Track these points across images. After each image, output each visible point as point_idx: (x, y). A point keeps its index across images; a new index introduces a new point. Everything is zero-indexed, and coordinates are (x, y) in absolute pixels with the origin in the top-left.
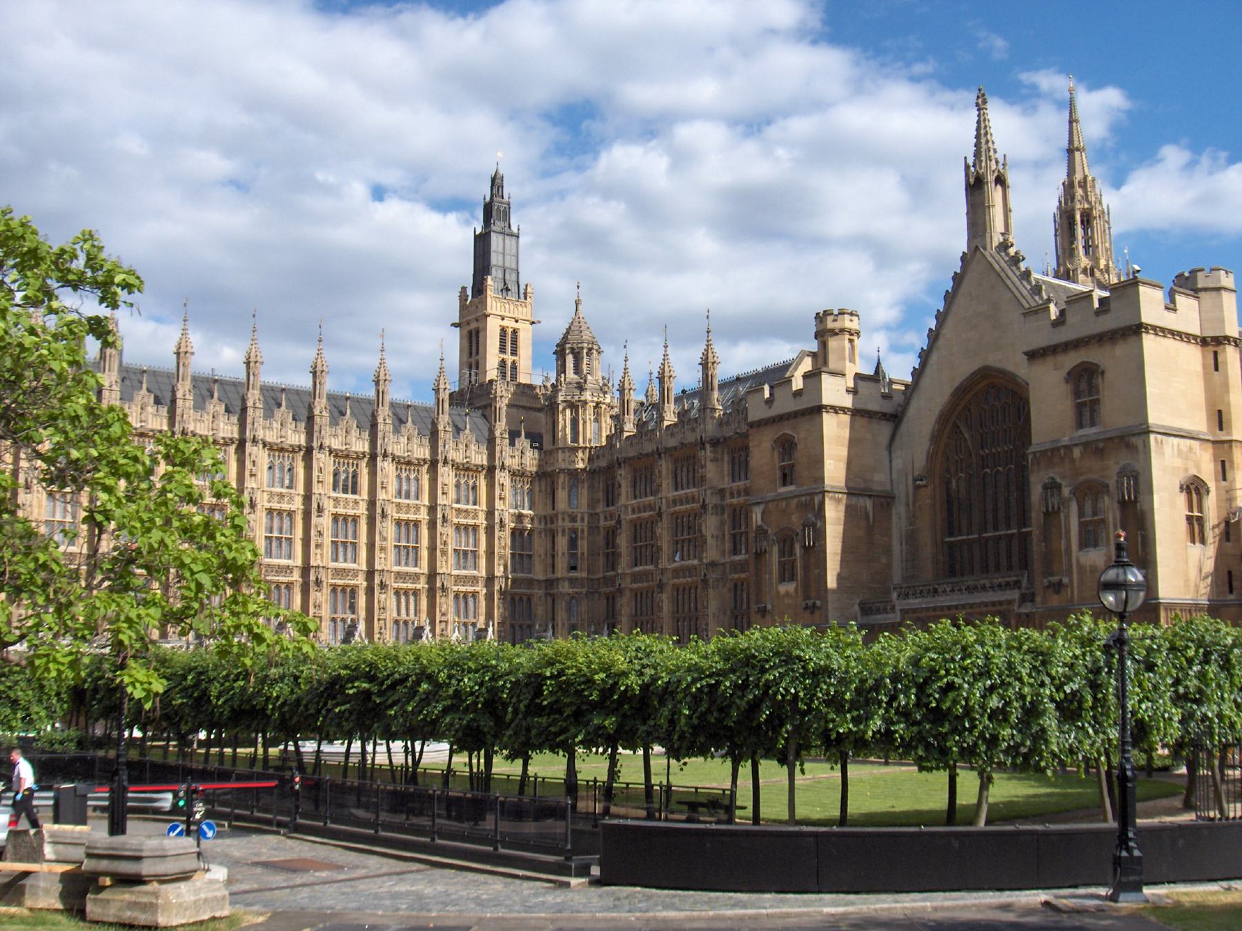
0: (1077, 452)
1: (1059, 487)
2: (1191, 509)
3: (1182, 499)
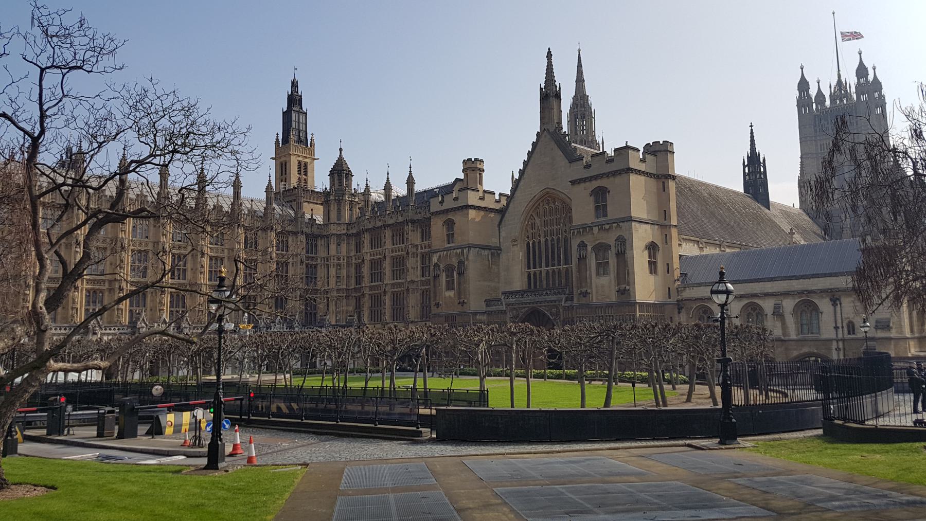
0: (596, 229)
2: (650, 257)
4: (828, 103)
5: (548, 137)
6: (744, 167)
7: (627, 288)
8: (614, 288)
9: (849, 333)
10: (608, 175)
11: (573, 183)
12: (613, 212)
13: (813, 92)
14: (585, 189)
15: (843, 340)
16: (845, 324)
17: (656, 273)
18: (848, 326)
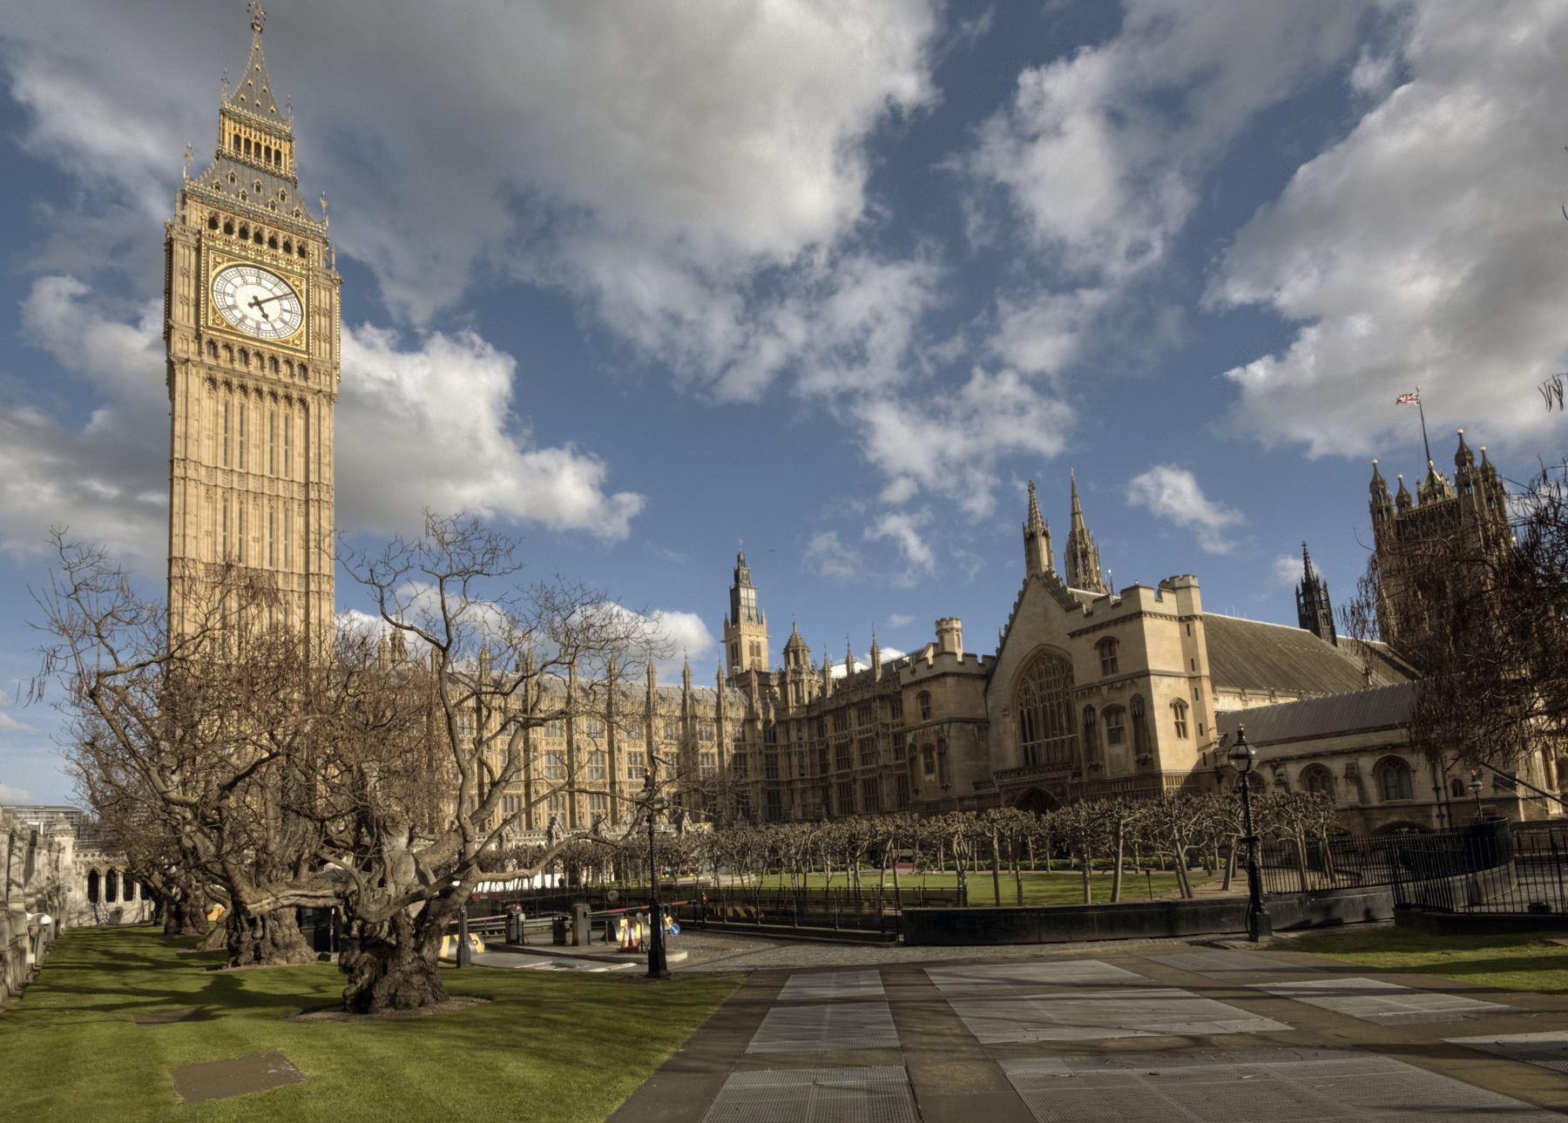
0: (1105, 690)
4: (1415, 505)
6: (1298, 596)
8: (1132, 758)
10: (1116, 622)
11: (1073, 635)
12: (1125, 667)
13: (1392, 492)
15: (1448, 804)
18: (1453, 786)
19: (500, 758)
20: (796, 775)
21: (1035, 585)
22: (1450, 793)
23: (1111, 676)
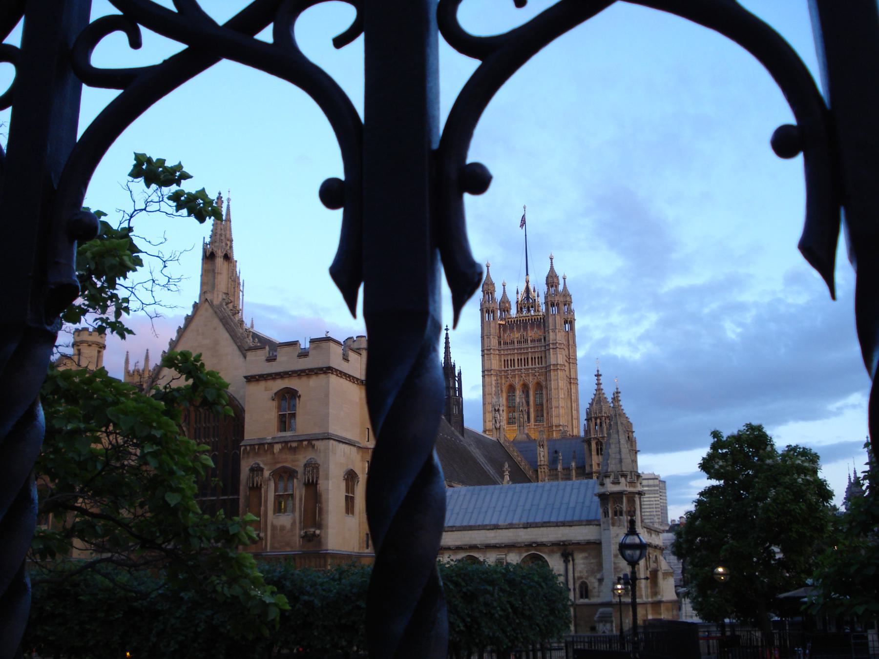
0: (277, 448)
1: (262, 470)
3: (343, 485)
4: (513, 312)
5: (210, 310)
7: (318, 532)
8: (298, 532)
9: (582, 597)
11: (250, 379)
12: (303, 425)
13: (498, 295)
14: (266, 389)
16: (577, 585)
17: (353, 513)
18: (581, 587)
19: (488, 555)
20: (760, 644)
21: (206, 312)
22: (578, 595)
23: (288, 434)
